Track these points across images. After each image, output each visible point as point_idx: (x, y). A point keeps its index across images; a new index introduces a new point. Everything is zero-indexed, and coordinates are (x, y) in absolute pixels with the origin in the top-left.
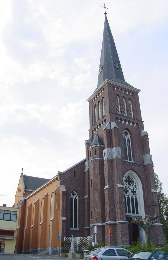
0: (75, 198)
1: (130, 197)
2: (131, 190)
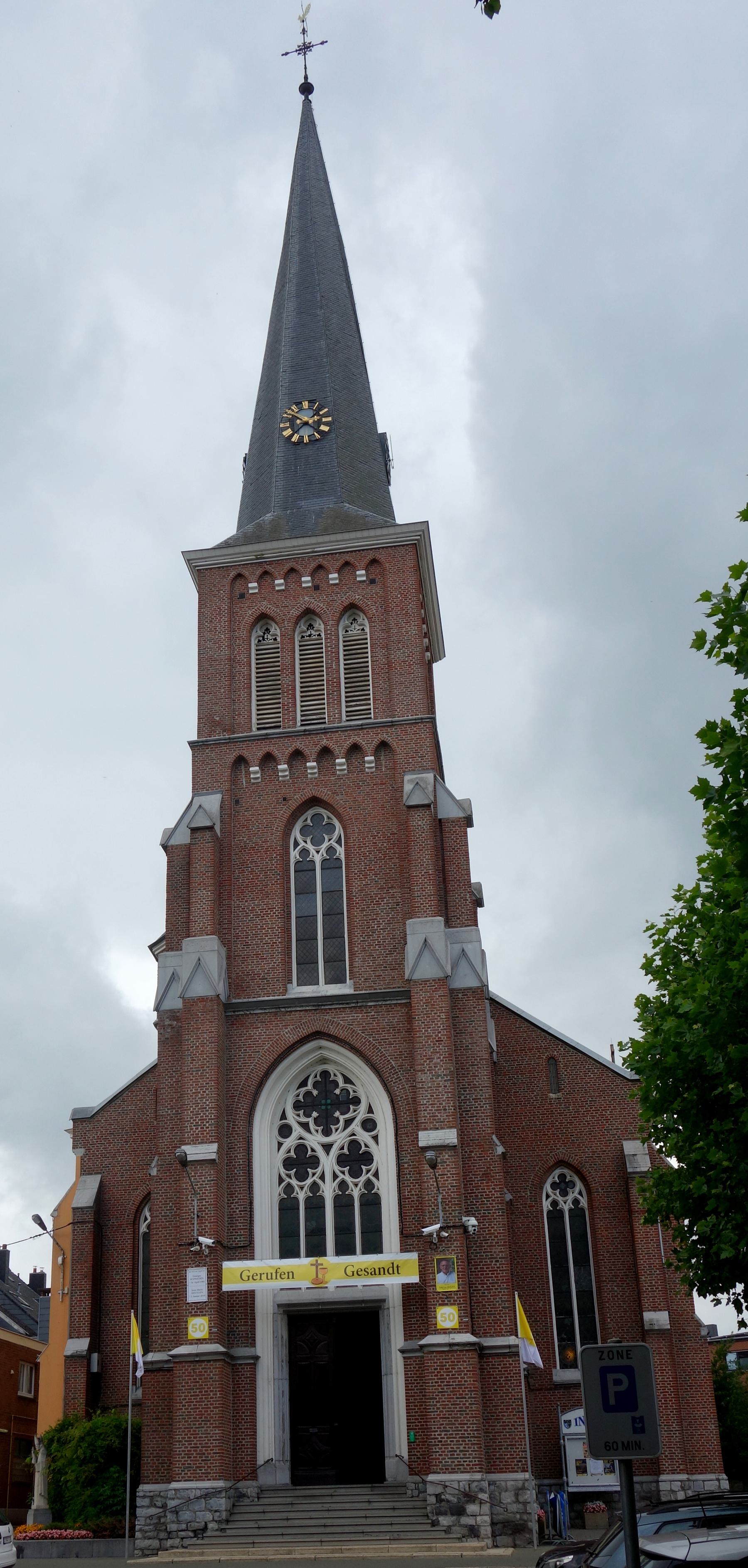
1: (329, 1191)
2: (334, 1151)
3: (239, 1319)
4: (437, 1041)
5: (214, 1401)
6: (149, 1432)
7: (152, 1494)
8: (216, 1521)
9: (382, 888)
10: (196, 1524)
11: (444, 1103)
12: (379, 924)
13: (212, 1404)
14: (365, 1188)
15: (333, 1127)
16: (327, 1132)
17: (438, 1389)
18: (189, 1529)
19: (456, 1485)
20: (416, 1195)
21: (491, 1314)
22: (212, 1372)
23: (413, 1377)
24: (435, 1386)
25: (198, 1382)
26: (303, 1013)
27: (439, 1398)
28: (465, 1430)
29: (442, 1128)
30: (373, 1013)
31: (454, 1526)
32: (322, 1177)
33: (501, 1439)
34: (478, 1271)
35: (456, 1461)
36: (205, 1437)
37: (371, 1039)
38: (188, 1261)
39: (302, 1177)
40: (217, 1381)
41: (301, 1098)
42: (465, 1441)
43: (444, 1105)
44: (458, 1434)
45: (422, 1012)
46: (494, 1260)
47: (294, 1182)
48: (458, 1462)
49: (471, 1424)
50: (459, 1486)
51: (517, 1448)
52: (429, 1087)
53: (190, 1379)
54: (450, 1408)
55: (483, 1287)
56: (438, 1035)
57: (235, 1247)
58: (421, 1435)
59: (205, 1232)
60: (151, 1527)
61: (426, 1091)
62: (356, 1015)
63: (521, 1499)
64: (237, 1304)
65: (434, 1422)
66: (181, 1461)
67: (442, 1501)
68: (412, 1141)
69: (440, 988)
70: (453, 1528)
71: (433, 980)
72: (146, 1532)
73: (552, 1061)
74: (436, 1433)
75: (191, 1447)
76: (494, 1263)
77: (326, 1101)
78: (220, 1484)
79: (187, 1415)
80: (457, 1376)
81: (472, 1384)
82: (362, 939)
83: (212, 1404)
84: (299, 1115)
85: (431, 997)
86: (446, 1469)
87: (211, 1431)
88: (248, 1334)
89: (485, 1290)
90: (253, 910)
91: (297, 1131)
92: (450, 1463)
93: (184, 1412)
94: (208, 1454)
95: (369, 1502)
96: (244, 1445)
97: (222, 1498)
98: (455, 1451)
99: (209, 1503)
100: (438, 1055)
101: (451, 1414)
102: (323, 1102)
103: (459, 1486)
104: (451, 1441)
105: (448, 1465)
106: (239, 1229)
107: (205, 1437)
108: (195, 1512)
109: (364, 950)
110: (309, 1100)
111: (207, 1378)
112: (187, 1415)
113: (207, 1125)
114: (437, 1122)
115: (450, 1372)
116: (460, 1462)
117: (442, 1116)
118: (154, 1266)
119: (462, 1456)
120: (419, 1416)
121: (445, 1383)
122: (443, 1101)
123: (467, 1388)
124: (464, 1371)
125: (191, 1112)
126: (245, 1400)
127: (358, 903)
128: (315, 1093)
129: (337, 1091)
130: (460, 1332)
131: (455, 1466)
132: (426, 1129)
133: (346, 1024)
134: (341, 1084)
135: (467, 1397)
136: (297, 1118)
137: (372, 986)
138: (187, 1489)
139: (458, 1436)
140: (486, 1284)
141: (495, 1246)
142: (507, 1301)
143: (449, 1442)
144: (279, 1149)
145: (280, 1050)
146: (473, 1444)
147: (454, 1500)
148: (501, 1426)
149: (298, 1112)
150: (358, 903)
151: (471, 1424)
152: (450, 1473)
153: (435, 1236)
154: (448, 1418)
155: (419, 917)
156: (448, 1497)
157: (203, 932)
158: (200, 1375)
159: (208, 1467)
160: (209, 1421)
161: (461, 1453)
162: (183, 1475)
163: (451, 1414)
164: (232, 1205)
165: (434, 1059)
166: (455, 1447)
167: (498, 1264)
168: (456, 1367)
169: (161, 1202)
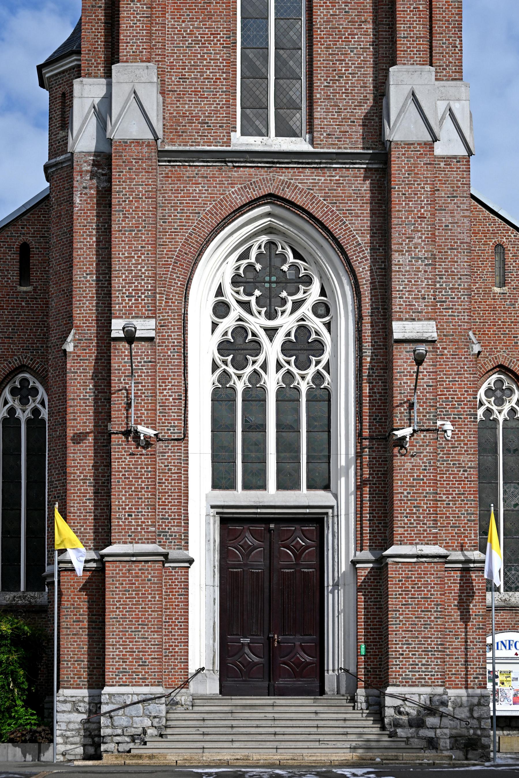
0: (36, 412)
2: (280, 338)
3: (172, 519)
4: (419, 217)
5: (151, 604)
6: (69, 635)
7: (74, 699)
8: (156, 727)
9: (353, 22)
10: (133, 729)
11: (423, 291)
12: (347, 67)
13: (151, 608)
14: (313, 382)
15: (279, 309)
16: (271, 315)
17: (402, 601)
18: (125, 733)
19: (416, 698)
20: (379, 393)
21: (456, 527)
22: (150, 574)
23: (367, 589)
24: (399, 598)
25: (135, 584)
26: (253, 169)
27: (403, 611)
28: (428, 644)
29: (419, 320)
30: (337, 178)
31: (412, 737)
32: (264, 366)
33: (458, 655)
34: (444, 481)
35: (417, 674)
36: (142, 642)
37: (334, 209)
38: (121, 452)
39: (240, 365)
40: (156, 584)
41: (241, 271)
42: (428, 655)
43: (423, 293)
44: (421, 648)
45: (403, 181)
46: (462, 470)
47: (231, 370)
48: (419, 675)
49: (435, 638)
50: (420, 699)
51: (474, 665)
52: (406, 271)
53: (126, 580)
54: (414, 621)
55: (448, 498)
56: (420, 211)
57: (168, 440)
58: (373, 649)
59: (141, 420)
60: (74, 733)
61: (403, 275)
62: (317, 178)
63: (476, 715)
64: (169, 502)
65: (396, 634)
66: (115, 665)
67: (400, 713)
68: (377, 332)
69: (426, 155)
70: (411, 740)
71: (418, 144)
72: (68, 737)
73: (499, 249)
74: (398, 646)
75: (126, 652)
76: (461, 472)
77: (270, 279)
78: (159, 690)
79: (121, 618)
80: (423, 589)
81: (439, 598)
82: (326, 84)
83: (151, 608)
84: (238, 293)
85: (416, 165)
86: (406, 682)
87: (149, 635)
88: (181, 535)
89: (450, 501)
90: (191, 33)
91: (236, 311)
92: (410, 676)
93: (119, 615)
94: (145, 659)
95: (316, 713)
96: (177, 652)
97: (161, 704)
98: (417, 665)
99: (148, 709)
100: (419, 234)
101: (415, 628)
102: (267, 279)
103: (420, 699)
104: (412, 655)
105: (408, 678)
106: (172, 420)
107: (142, 642)
108: (132, 717)
109: (328, 98)
110: (251, 275)
111: (145, 580)
112: (121, 618)
113: (143, 296)
114: (414, 312)
115: (416, 584)
116: (422, 675)
117: (420, 305)
118: (72, 455)
119: (423, 670)
120: (371, 629)
121: (410, 596)
122: (422, 288)
123: (433, 601)
124: (431, 584)
125: (123, 280)
126: (178, 605)
127: (323, 38)
128: (258, 267)
129: (285, 268)
130: (428, 544)
131: (416, 679)
132: (401, 319)
133: (305, 188)
134: (291, 258)
135: (433, 610)
136: (237, 296)
137: (337, 144)
138: (123, 694)
139: (420, 650)
140: (452, 494)
141: (464, 454)
142: (473, 514)
143: (411, 655)
144: (213, 331)
145: (225, 213)
146: (437, 658)
147: (414, 713)
148: (459, 642)
149: (238, 289)
150: (323, 38)
151: (435, 638)
152: (410, 686)
153: (408, 439)
154: (412, 631)
155: (405, 64)
156: (407, 709)
157: (135, 58)
158: (137, 577)
159: (145, 672)
160: (147, 625)
161: (423, 667)
162: (117, 680)
163: (415, 628)
164: (165, 392)
165: (414, 238)
166: (417, 660)
167: (466, 473)
168: (423, 580)
169: (79, 383)
